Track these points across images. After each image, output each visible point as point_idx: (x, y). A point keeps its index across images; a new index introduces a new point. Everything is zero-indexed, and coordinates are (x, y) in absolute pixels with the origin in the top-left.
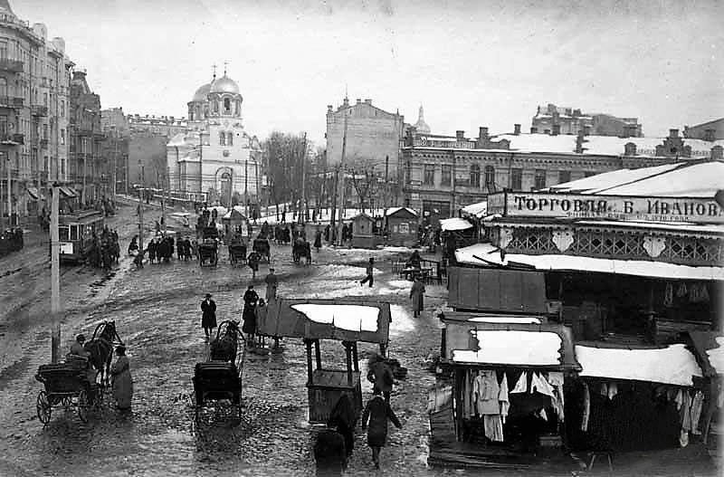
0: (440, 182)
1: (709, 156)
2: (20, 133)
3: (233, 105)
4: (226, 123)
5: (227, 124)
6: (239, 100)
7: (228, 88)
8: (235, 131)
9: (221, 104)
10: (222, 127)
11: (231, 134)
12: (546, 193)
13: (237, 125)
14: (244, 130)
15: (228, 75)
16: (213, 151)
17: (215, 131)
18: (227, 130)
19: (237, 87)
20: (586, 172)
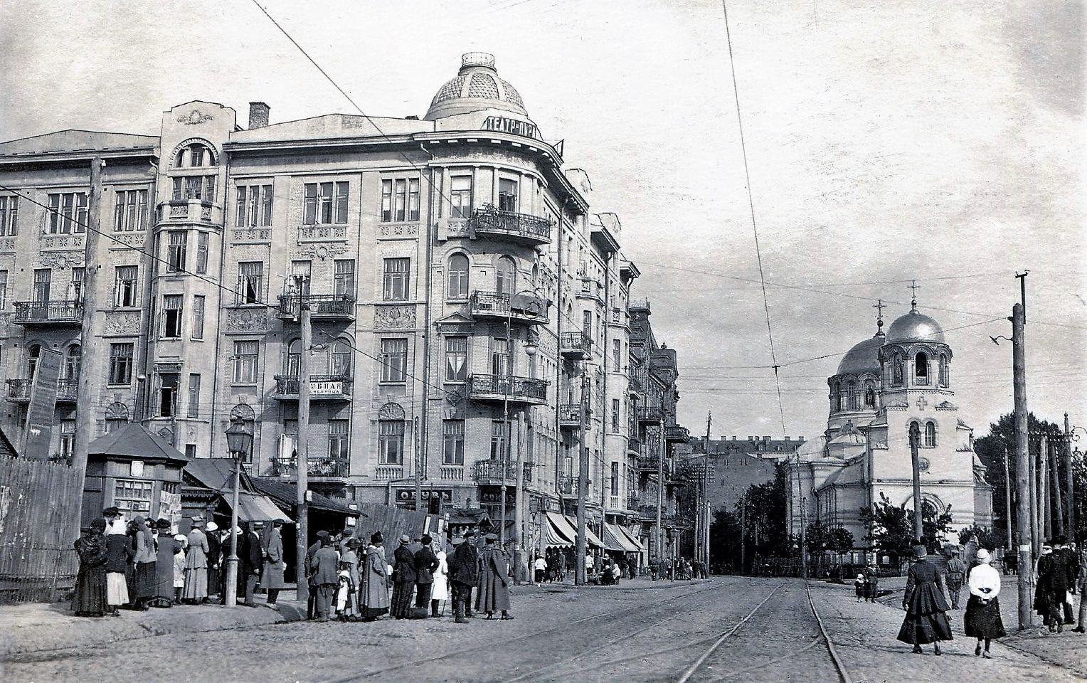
0: (518, 492)
1: (280, 592)
2: (540, 377)
3: (934, 365)
4: (917, 403)
5: (922, 404)
6: (946, 355)
7: (923, 332)
8: (938, 416)
9: (910, 366)
10: (914, 412)
11: (931, 424)
12: (606, 300)
13: (944, 406)
14: (959, 414)
15: (920, 310)
16: (891, 462)
17: (898, 423)
18: (923, 416)
19: (939, 330)
20: (479, 571)
